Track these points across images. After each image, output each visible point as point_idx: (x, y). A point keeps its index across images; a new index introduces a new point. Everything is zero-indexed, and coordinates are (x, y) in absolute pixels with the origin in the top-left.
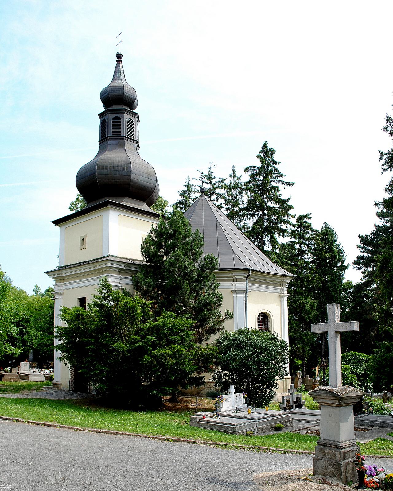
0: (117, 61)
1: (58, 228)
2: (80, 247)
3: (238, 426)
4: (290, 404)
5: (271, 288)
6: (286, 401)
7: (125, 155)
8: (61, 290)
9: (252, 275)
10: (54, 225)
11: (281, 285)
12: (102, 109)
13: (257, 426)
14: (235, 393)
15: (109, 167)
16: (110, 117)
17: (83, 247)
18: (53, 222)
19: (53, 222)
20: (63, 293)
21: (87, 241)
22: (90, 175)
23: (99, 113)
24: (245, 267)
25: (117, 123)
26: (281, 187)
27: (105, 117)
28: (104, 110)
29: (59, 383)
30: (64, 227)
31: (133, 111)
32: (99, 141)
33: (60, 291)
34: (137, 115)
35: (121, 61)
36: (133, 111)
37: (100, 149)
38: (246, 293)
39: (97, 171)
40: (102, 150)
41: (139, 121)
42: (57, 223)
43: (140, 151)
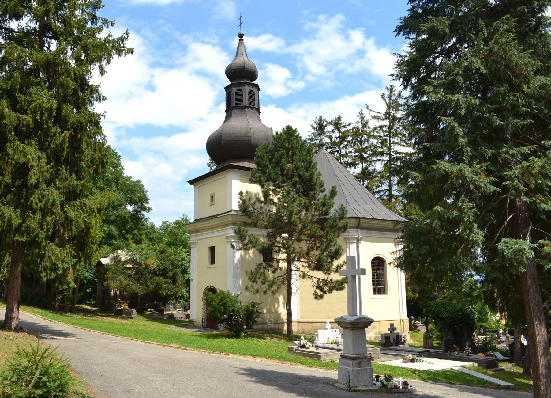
1: (193, 186)
7: (246, 123)
14: (330, 328)
16: (234, 90)
18: (189, 182)
19: (189, 182)
21: (216, 198)
23: (225, 86)
24: (356, 216)
25: (240, 94)
28: (230, 83)
29: (194, 320)
30: (198, 186)
31: (254, 82)
32: (225, 111)
34: (257, 86)
36: (254, 82)
40: (228, 117)
41: (260, 90)
42: (192, 182)
43: (261, 116)
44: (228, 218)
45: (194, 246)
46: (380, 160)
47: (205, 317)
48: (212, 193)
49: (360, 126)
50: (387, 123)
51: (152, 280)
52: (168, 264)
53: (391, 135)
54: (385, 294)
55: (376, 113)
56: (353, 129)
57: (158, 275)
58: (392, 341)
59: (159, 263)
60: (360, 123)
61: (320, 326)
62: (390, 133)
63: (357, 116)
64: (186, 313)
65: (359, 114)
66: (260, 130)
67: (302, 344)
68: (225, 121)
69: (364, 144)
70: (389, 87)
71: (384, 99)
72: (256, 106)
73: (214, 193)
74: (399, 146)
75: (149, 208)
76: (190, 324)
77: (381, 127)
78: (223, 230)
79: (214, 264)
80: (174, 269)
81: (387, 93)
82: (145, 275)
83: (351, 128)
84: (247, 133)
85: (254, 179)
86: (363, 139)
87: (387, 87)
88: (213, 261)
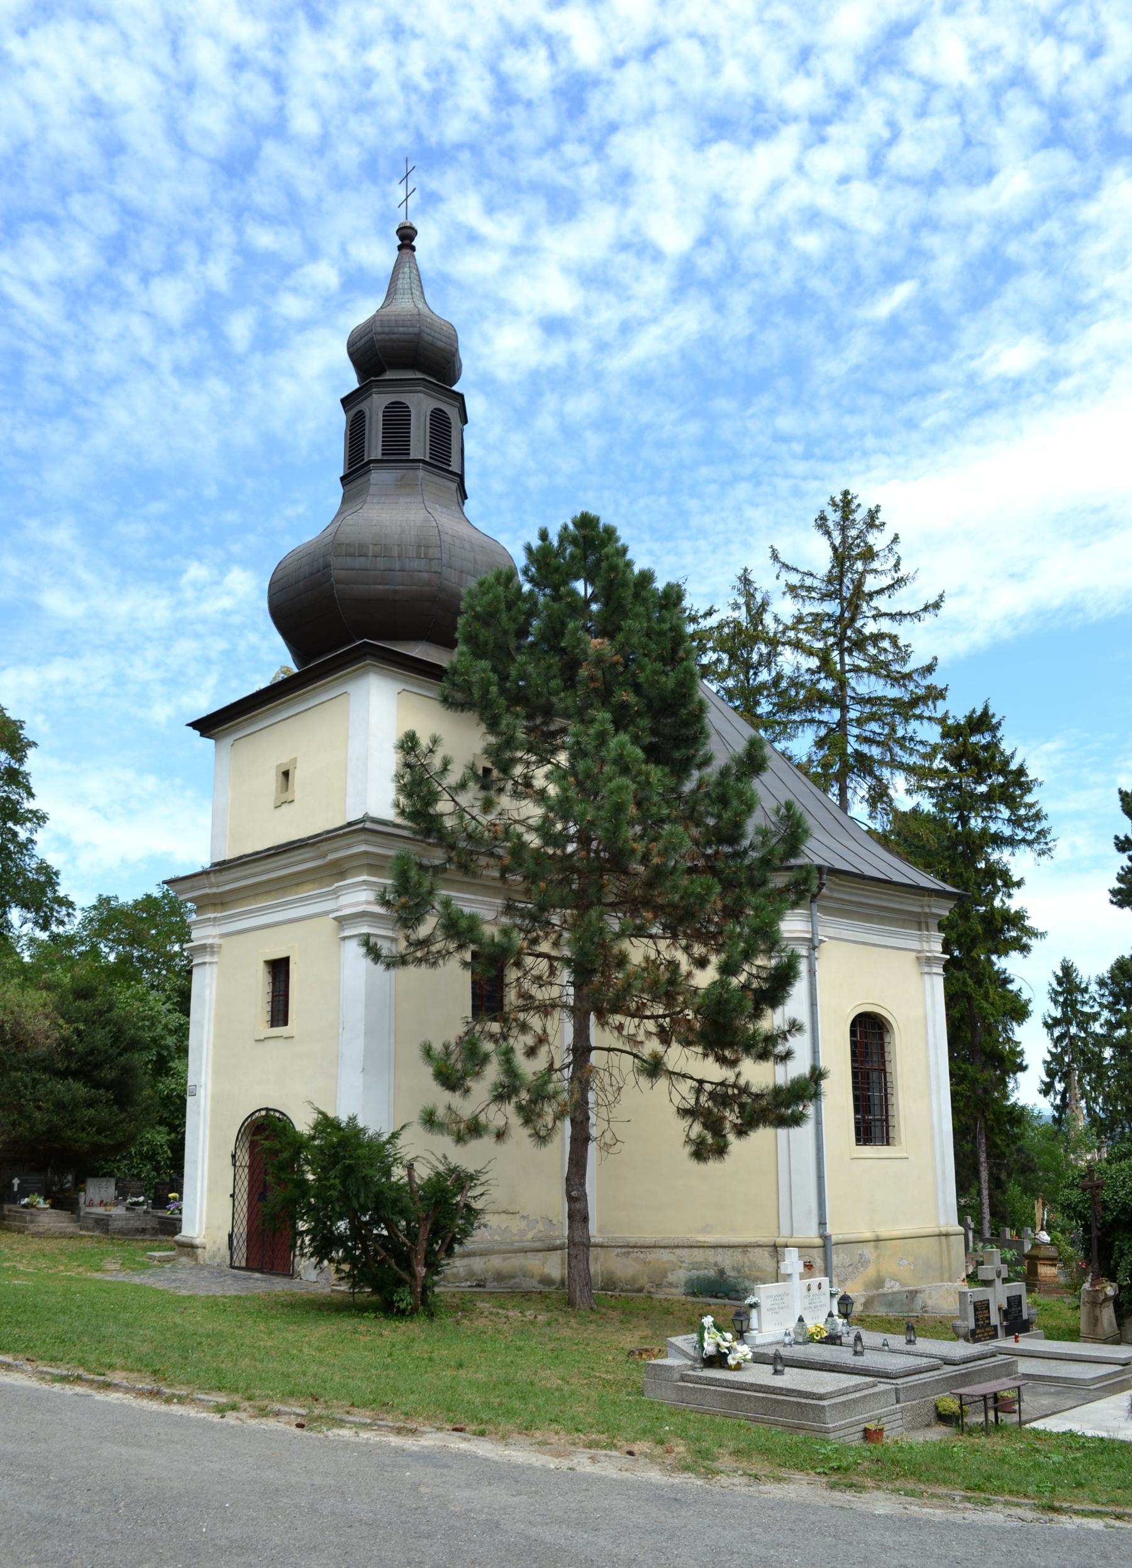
0: (400, 248)
1: (210, 743)
2: (276, 799)
3: (833, 1401)
4: (989, 1318)
5: (891, 932)
6: (976, 1309)
8: (214, 937)
9: (831, 890)
10: (198, 733)
11: (919, 922)
12: (352, 382)
13: (898, 1402)
15: (371, 547)
16: (378, 403)
17: (284, 797)
18: (195, 725)
19: (195, 725)
20: (220, 946)
21: (297, 777)
22: (312, 574)
25: (397, 418)
26: (905, 632)
27: (364, 406)
29: (197, 1241)
30: (229, 740)
33: (209, 941)
35: (413, 249)
37: (345, 500)
38: (814, 948)
39: (333, 561)
42: (208, 726)
44: (349, 846)
45: (207, 959)
46: (812, 721)
47: (242, 1229)
48: (284, 759)
49: (742, 615)
50: (832, 607)
51: (41, 1091)
52: (101, 1036)
53: (846, 644)
54: (888, 1144)
55: (799, 576)
56: (720, 627)
57: (63, 1075)
58: (995, 1319)
59: (66, 1033)
60: (744, 609)
61: (673, 1258)
62: (843, 638)
63: (734, 588)
64: (161, 1213)
65: (737, 583)
66: (471, 543)
67: (710, 1349)
68: (339, 514)
69: (755, 674)
70: (838, 498)
71: (828, 533)
72: (454, 467)
73: (294, 760)
74: (873, 677)
75: (34, 813)
76: (181, 1254)
77: (818, 618)
78: (327, 894)
79: (286, 1024)
80: (120, 1054)
81: (834, 517)
82: (13, 1074)
83: (715, 625)
84: (427, 547)
85: (459, 696)
86: (755, 657)
87: (832, 499)
88: (279, 1014)
